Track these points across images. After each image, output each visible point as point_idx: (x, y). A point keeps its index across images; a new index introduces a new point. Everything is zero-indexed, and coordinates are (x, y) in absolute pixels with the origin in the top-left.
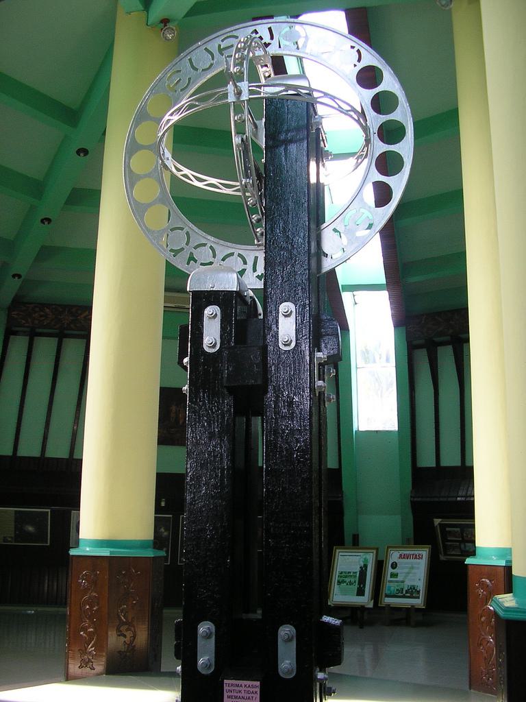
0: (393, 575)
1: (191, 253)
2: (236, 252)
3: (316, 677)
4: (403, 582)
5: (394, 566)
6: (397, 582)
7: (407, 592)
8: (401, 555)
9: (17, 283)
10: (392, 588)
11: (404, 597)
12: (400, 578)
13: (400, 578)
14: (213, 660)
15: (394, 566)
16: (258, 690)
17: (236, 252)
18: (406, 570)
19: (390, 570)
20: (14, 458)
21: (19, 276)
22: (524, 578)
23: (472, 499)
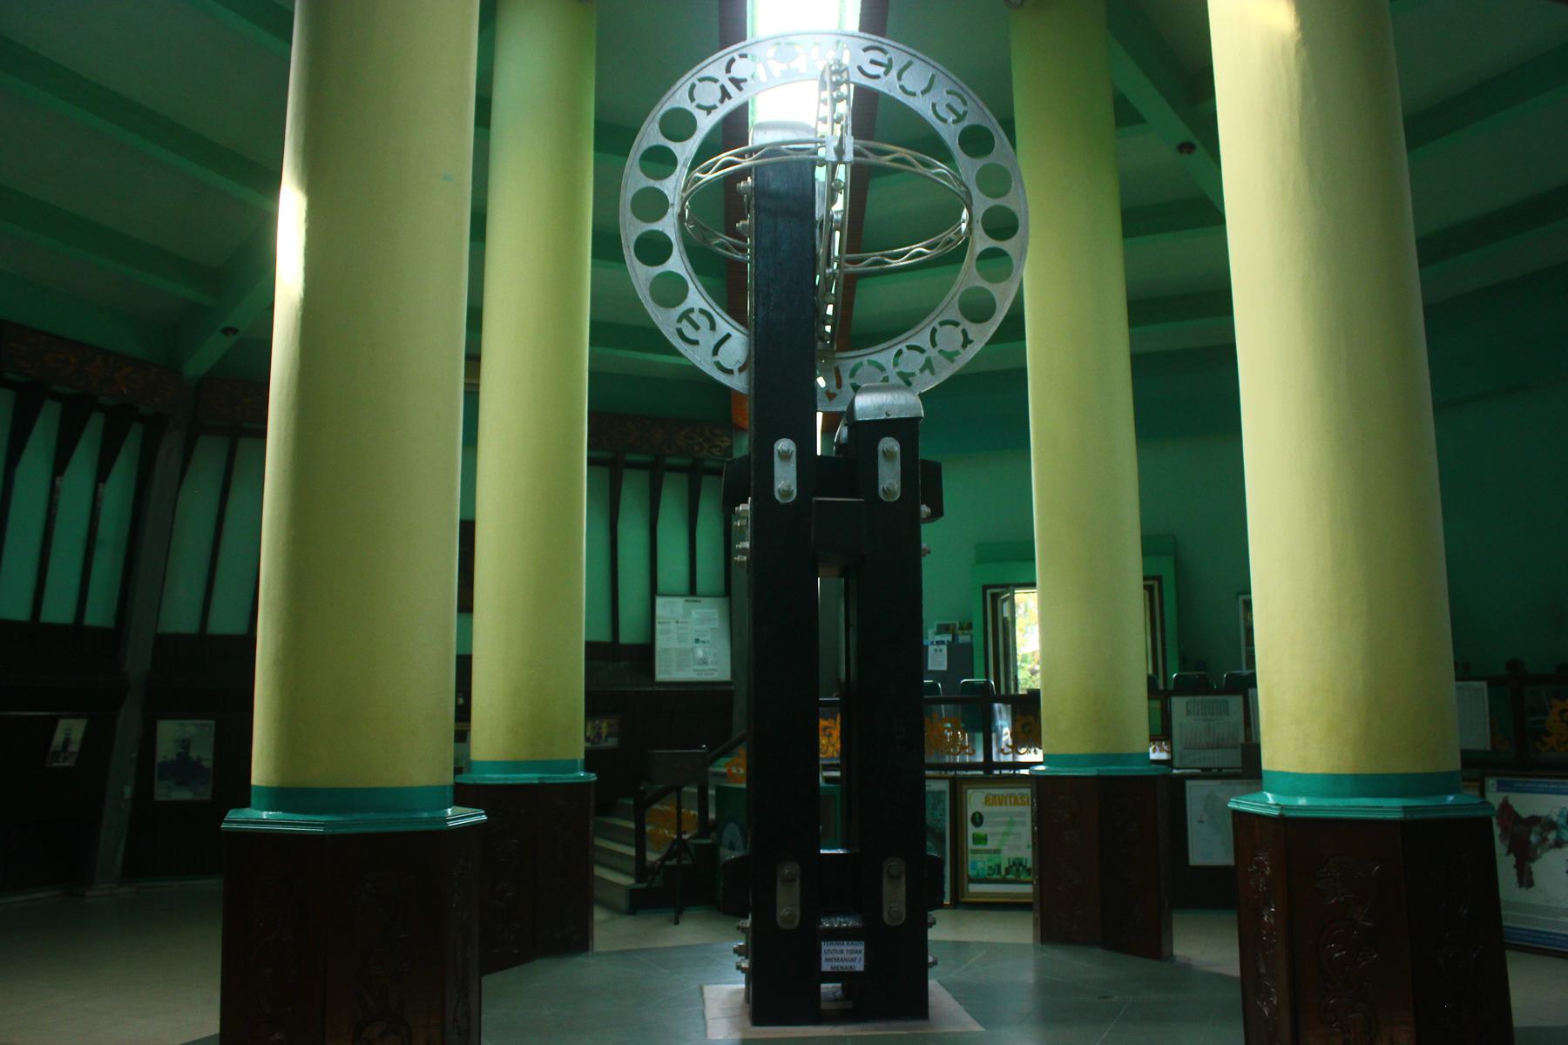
0: (979, 839)
1: (900, 374)
2: (935, 324)
3: (1491, 775)
4: (997, 852)
5: (978, 820)
6: (988, 852)
7: (1008, 871)
8: (987, 798)
9: (226, 342)
10: (980, 865)
11: (1004, 881)
12: (991, 845)
13: (991, 845)
14: (798, 913)
15: (978, 820)
16: (862, 956)
17: (935, 324)
18: (1002, 829)
19: (971, 829)
20: (33, 631)
21: (235, 331)
22: (1225, 979)
23: (596, 454)
